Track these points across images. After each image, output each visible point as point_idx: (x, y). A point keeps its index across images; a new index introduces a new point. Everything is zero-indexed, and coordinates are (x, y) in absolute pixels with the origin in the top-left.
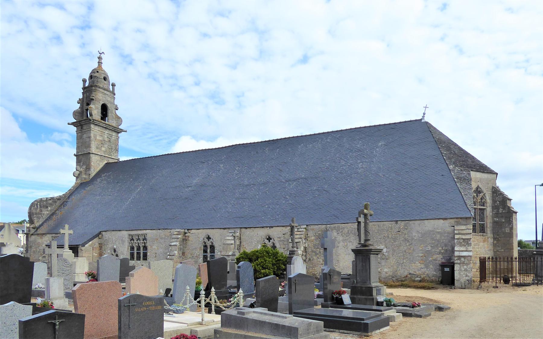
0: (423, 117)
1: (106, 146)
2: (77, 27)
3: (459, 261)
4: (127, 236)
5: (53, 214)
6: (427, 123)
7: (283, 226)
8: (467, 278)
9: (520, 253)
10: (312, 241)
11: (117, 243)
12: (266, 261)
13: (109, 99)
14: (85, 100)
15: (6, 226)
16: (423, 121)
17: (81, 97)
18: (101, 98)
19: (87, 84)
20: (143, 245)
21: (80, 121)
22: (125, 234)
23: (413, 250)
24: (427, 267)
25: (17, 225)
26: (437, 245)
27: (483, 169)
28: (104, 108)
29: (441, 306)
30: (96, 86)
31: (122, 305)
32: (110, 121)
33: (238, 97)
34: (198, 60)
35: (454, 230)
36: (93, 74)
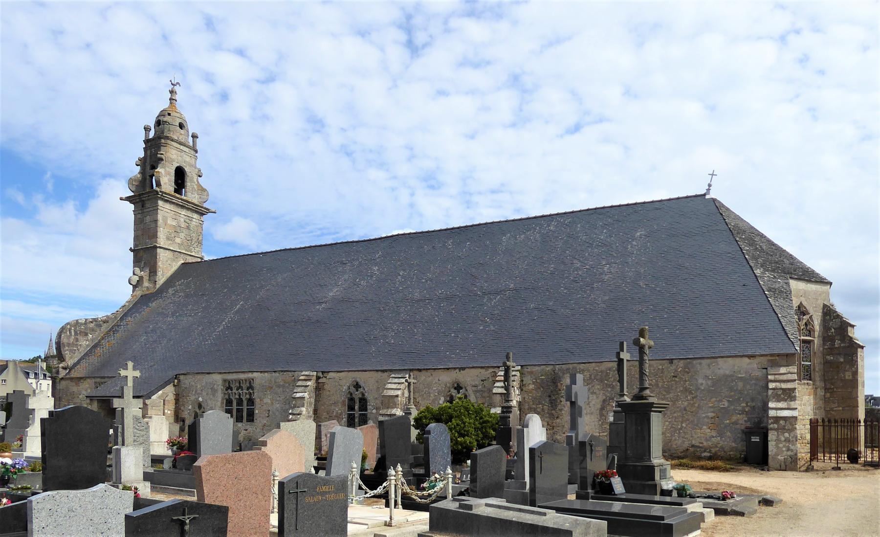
0: (708, 190)
1: (182, 235)
2: (258, 81)
3: (776, 426)
4: (220, 382)
5: (95, 346)
6: (714, 200)
7: (482, 368)
8: (789, 453)
9: (868, 412)
10: (531, 392)
11: (204, 393)
12: (464, 423)
13: (188, 159)
14: (148, 161)
15: (11, 366)
16: (707, 197)
17: (142, 155)
18: (174, 157)
19: (152, 134)
20: (248, 396)
21: (140, 195)
22: (218, 378)
23: (699, 407)
24: (721, 434)
25: (26, 365)
26: (739, 398)
27: (809, 276)
28: (180, 175)
29: (768, 497)
30: (167, 138)
31: (286, 491)
32: (189, 194)
35: (767, 374)
36: (161, 118)
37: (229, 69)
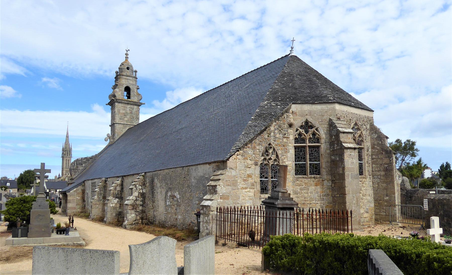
1: (128, 117)
2: (254, 29)
27: (345, 99)
28: (128, 89)
33: (378, 53)
34: (345, 31)
37: (240, 27)
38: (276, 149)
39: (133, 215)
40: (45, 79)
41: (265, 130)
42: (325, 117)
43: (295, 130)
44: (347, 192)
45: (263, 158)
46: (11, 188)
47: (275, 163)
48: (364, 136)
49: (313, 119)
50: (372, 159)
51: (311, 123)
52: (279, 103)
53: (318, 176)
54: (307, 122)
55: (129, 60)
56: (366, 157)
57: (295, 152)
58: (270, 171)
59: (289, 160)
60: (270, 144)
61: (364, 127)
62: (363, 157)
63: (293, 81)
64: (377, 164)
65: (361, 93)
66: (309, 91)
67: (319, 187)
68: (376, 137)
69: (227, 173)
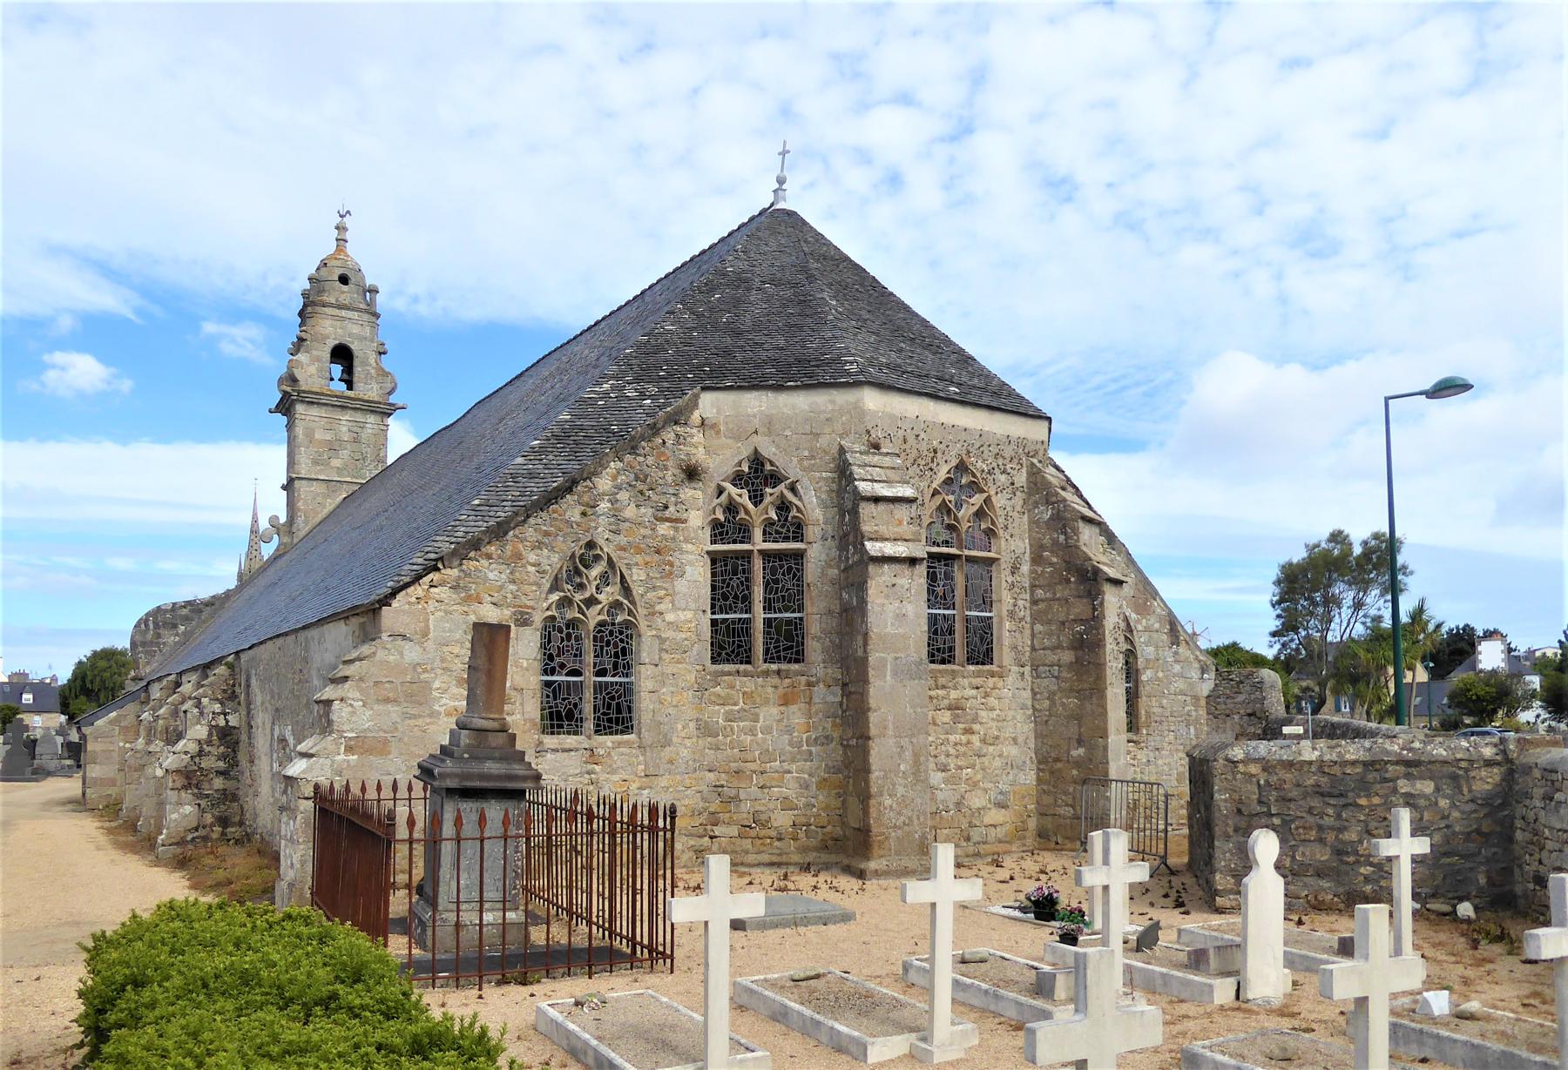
1: (345, 453)
2: (942, 140)
6: (791, 214)
28: (342, 354)
33: (1391, 220)
37: (891, 131)
38: (621, 565)
39: (188, 809)
40: (210, 328)
41: (569, 488)
42: (823, 442)
43: (711, 489)
44: (873, 731)
45: (555, 597)
46: (39, 712)
47: (619, 619)
48: (999, 512)
49: (778, 447)
50: (1034, 602)
51: (772, 464)
52: (652, 389)
53: (795, 667)
54: (757, 461)
55: (350, 248)
56: (1007, 598)
57: (713, 575)
58: (588, 645)
59: (679, 608)
60: (591, 545)
61: (1003, 478)
62: (994, 597)
63: (772, 304)
64: (1049, 622)
65: (1326, 367)
66: (782, 343)
67: (794, 708)
68: (1047, 516)
69: (381, 654)
